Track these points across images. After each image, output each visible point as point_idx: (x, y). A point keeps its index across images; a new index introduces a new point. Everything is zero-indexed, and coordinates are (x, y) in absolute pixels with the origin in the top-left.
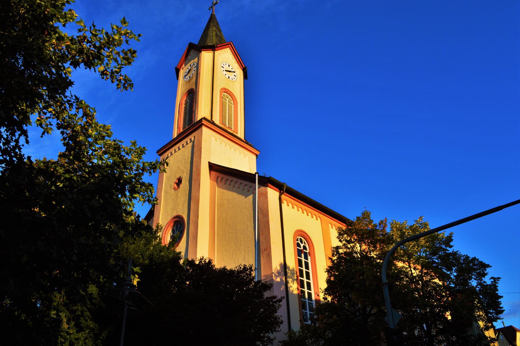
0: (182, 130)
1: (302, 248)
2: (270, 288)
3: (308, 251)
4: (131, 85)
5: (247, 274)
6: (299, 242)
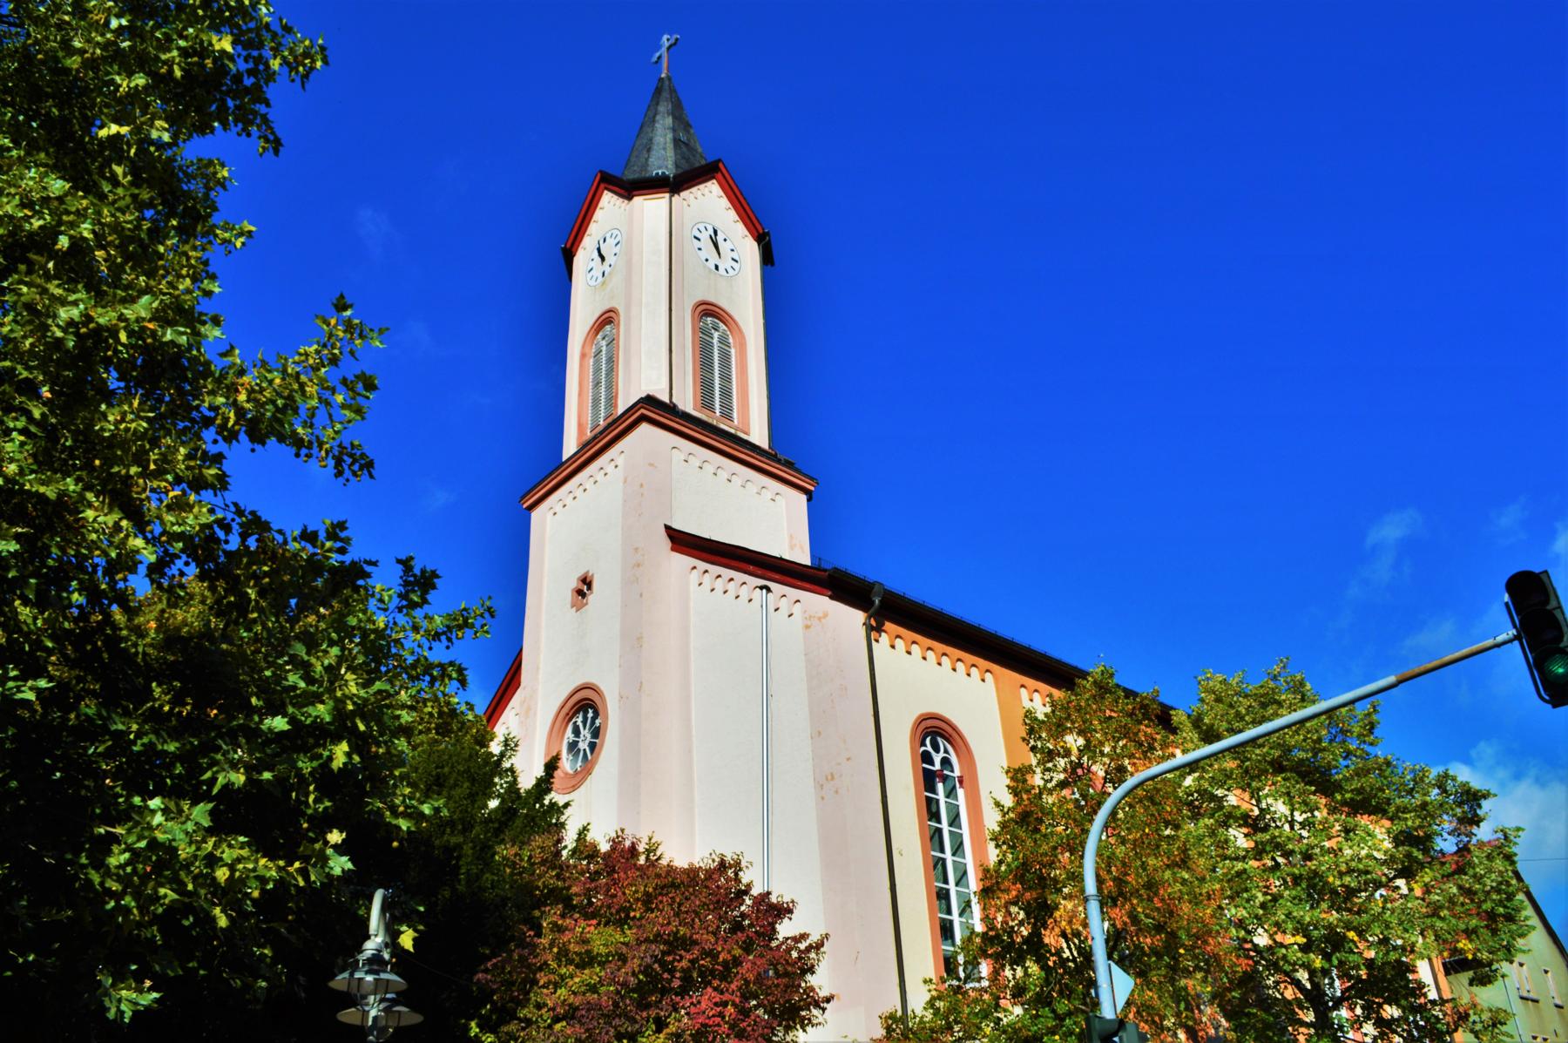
0: (589, 435)
1: (937, 766)
2: (790, 911)
3: (957, 773)
4: (342, 526)
5: (728, 880)
6: (929, 748)
